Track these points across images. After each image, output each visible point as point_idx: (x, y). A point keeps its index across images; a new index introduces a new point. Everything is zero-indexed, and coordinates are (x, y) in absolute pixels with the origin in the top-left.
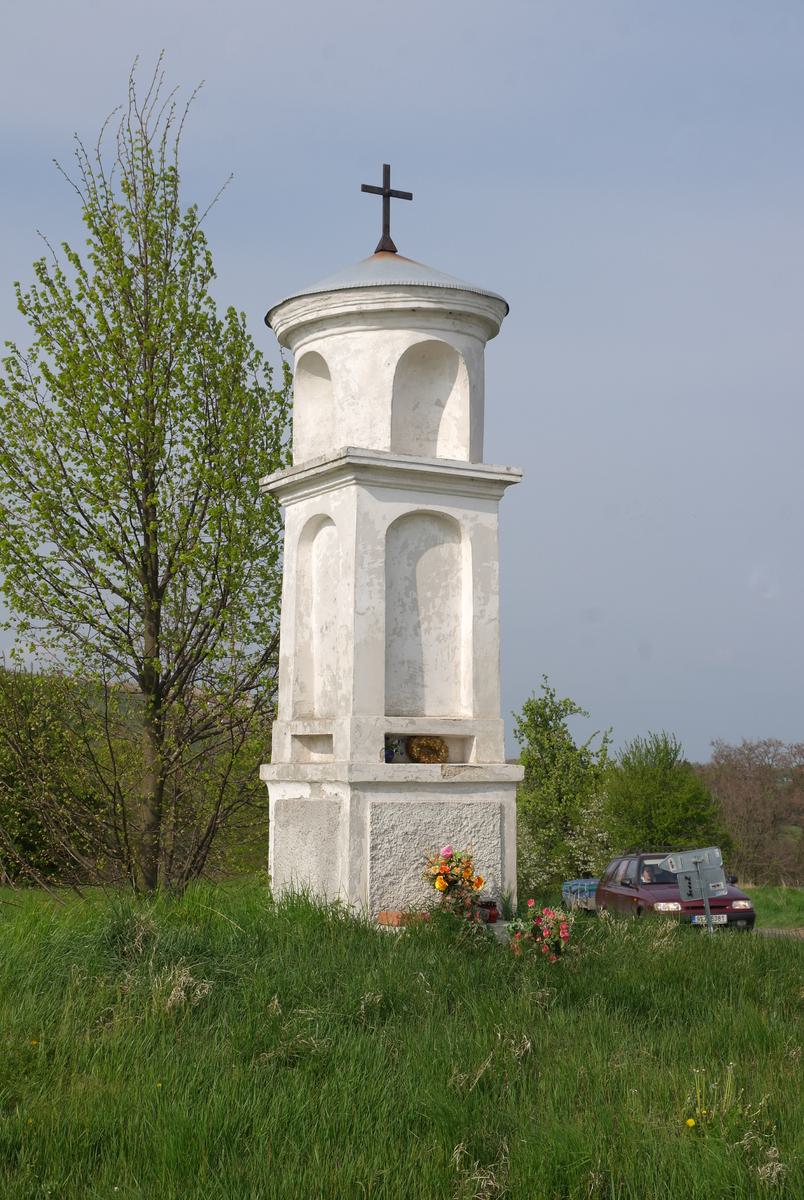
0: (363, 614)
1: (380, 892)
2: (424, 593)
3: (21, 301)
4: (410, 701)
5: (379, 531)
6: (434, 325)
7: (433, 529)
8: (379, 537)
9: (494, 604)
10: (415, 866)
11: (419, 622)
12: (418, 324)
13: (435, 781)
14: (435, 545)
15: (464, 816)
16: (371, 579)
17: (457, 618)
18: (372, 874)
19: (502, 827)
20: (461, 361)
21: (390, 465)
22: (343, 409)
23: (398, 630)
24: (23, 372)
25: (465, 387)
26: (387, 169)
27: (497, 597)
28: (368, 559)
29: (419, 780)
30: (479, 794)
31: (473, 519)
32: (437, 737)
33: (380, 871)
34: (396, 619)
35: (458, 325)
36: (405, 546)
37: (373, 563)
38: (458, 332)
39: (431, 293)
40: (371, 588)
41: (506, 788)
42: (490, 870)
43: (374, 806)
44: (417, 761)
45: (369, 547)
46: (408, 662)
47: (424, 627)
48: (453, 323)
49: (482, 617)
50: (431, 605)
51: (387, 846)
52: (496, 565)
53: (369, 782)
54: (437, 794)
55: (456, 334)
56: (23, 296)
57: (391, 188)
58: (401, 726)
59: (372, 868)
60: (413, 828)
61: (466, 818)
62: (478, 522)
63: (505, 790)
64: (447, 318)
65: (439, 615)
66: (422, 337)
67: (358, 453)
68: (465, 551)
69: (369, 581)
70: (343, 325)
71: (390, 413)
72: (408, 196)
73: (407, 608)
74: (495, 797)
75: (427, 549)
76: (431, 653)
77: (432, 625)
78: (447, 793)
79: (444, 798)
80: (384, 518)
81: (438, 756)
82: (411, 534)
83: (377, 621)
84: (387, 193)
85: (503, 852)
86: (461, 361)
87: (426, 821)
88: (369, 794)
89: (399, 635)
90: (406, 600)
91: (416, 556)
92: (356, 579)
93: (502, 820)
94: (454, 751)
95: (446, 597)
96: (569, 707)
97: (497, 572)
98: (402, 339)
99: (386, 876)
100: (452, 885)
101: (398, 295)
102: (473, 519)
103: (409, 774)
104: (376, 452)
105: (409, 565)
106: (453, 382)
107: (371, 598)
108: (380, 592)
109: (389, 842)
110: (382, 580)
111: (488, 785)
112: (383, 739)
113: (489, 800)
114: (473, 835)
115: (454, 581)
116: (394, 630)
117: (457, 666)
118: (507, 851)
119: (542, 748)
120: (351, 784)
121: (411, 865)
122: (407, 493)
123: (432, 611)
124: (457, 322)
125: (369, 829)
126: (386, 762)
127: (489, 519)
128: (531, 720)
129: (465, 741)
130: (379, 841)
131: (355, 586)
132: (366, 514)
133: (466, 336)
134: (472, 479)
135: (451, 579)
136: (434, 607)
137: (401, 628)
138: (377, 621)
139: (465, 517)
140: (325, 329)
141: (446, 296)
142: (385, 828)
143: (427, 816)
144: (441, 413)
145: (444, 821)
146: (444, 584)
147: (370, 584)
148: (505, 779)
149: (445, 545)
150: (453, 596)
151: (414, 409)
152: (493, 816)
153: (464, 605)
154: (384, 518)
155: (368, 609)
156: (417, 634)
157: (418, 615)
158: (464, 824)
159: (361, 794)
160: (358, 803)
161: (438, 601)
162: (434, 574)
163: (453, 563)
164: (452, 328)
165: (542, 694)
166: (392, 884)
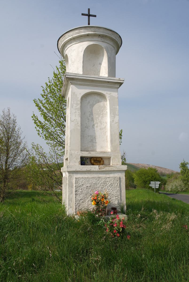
0: (73, 121)
1: (78, 205)
2: (95, 116)
3: (50, 81)
4: (91, 147)
5: (78, 98)
6: (95, 39)
7: (98, 98)
8: (78, 99)
9: (117, 119)
10: (90, 197)
11: (94, 124)
12: (90, 39)
13: (97, 170)
14: (99, 102)
15: (107, 181)
16: (76, 111)
17: (106, 123)
18: (76, 199)
19: (120, 184)
20: (105, 50)
21: (80, 78)
22: (71, 66)
23: (87, 127)
24: (45, 92)
25: (106, 57)
26: (89, 10)
27: (118, 116)
28: (75, 105)
29: (91, 170)
30: (112, 174)
31: (109, 94)
32: (100, 158)
33: (78, 198)
34: (86, 124)
35: (103, 40)
36: (89, 102)
37: (76, 107)
38: (103, 41)
39: (92, 29)
40: (76, 114)
41: (121, 172)
42: (116, 198)
43: (76, 178)
44: (93, 164)
45: (75, 102)
46: (91, 136)
47: (95, 126)
48: (101, 39)
49: (113, 122)
50: (98, 119)
51: (81, 190)
52: (117, 107)
53: (74, 171)
54: (98, 174)
55: (102, 42)
56: (50, 80)
57: (90, 14)
58: (86, 154)
59: (75, 197)
60: (89, 185)
61: (108, 182)
62: (111, 95)
63: (121, 173)
64: (99, 37)
65: (100, 122)
66: (91, 43)
67: (69, 74)
68: (108, 104)
69: (75, 112)
70: (71, 44)
71: (82, 65)
72: (95, 16)
73: (90, 120)
74: (117, 175)
75: (96, 104)
76: (98, 133)
77: (98, 125)
78: (102, 174)
79: (100, 175)
80: (80, 94)
81: (100, 163)
82: (90, 99)
83: (78, 123)
84: (89, 15)
85: (121, 191)
86: (105, 50)
87: (94, 183)
88: (75, 175)
89: (87, 128)
90: (89, 118)
91: (92, 106)
92: (71, 111)
93: (120, 182)
94: (106, 162)
95: (103, 117)
96: (187, 163)
97: (118, 109)
98: (85, 44)
99: (80, 200)
100: (97, 203)
101: (82, 30)
102: (109, 94)
103: (88, 169)
104: (75, 74)
105: (90, 108)
106: (103, 57)
107: (76, 117)
108: (79, 115)
109: (81, 189)
110: (79, 111)
111: (115, 172)
112: (80, 158)
113: (116, 176)
114: (110, 187)
115: (105, 112)
116: (86, 126)
117: (107, 137)
118: (122, 191)
119: (184, 170)
120: (68, 172)
121: (89, 196)
122: (88, 86)
123: (98, 121)
124: (102, 39)
125: (74, 185)
126: (81, 165)
127: (114, 94)
128: (182, 165)
129: (109, 158)
130: (78, 189)
131: (70, 113)
132: (74, 93)
133: (106, 43)
134: (108, 82)
135: (104, 112)
136: (99, 120)
137: (88, 126)
138: (78, 123)
139: (107, 93)
140: (67, 47)
141: (97, 30)
142: (80, 185)
143: (94, 181)
144: (101, 66)
145: (100, 183)
146: (102, 113)
147: (75, 112)
148: (121, 169)
149: (102, 102)
150: (105, 117)
151: (93, 66)
152: (117, 181)
153: (108, 119)
154: (80, 94)
155: (75, 120)
156: (93, 128)
157: (94, 122)
158: (107, 183)
159: (72, 175)
160: (71, 177)
161: (100, 118)
162: (99, 111)
163: (105, 107)
164: (101, 40)
165: (183, 162)
166: (83, 202)
